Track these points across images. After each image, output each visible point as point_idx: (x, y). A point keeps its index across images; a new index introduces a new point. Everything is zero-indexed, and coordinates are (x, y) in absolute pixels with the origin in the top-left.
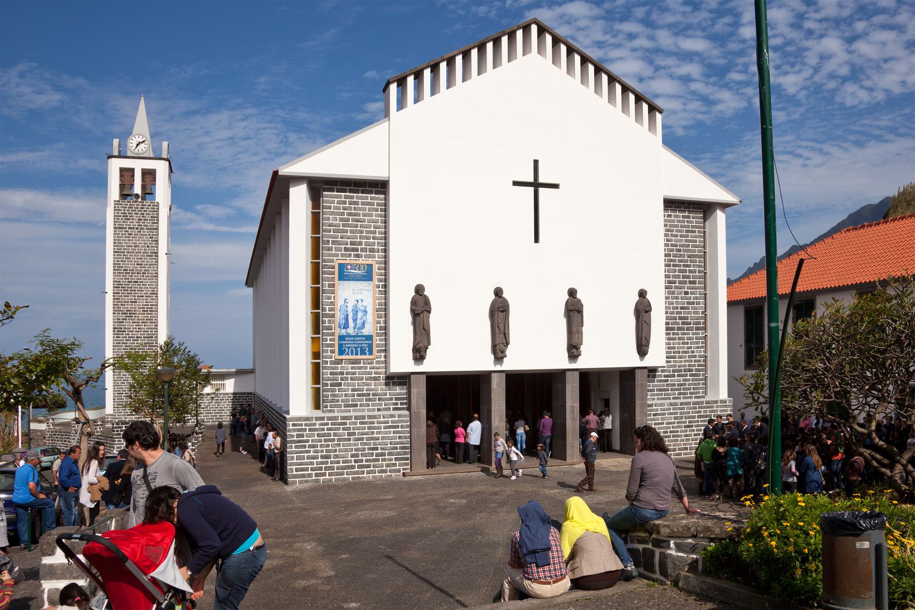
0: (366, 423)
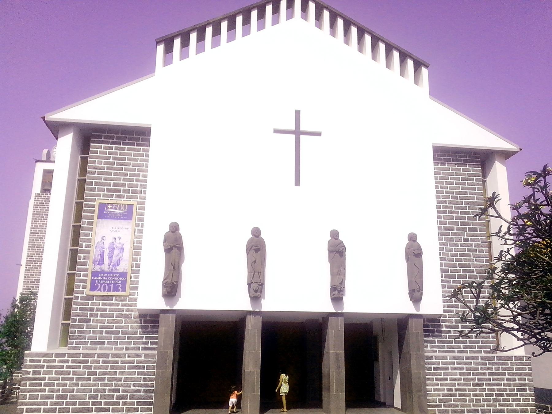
0: (108, 362)
